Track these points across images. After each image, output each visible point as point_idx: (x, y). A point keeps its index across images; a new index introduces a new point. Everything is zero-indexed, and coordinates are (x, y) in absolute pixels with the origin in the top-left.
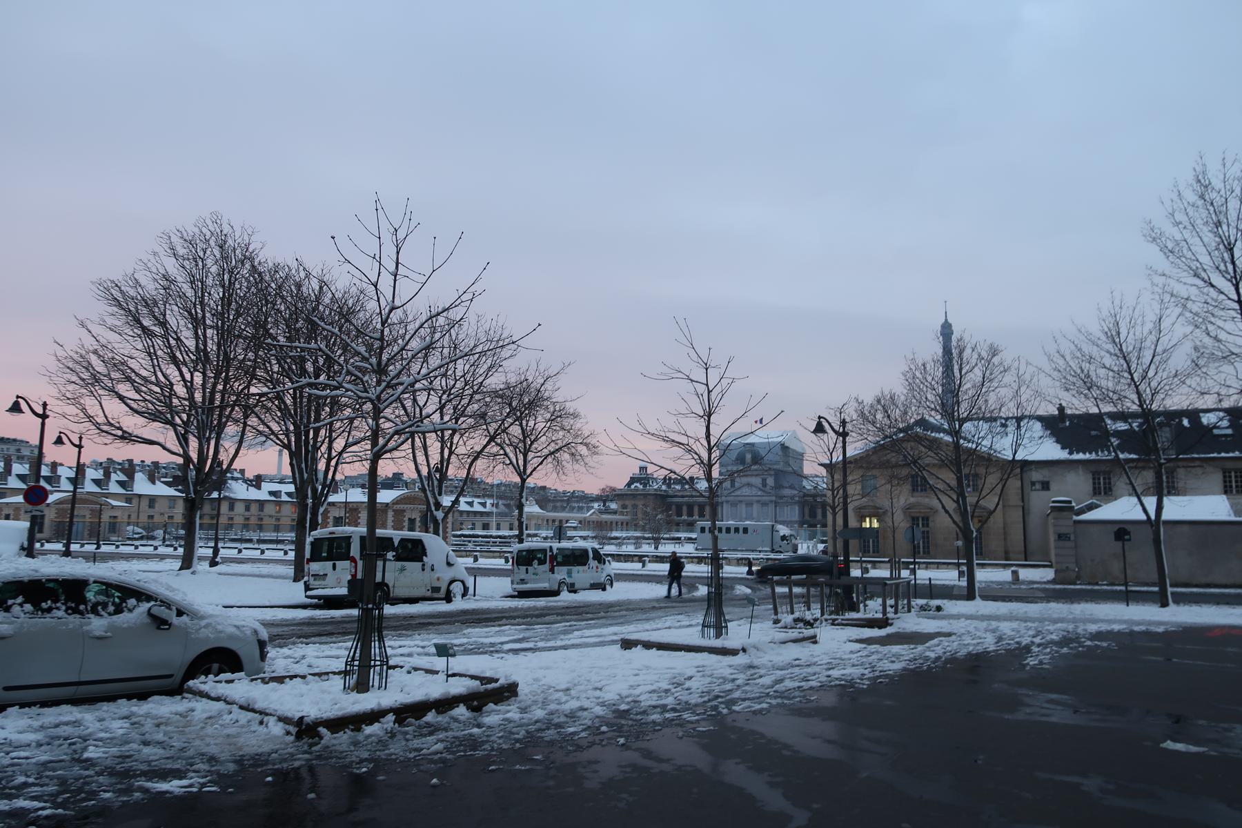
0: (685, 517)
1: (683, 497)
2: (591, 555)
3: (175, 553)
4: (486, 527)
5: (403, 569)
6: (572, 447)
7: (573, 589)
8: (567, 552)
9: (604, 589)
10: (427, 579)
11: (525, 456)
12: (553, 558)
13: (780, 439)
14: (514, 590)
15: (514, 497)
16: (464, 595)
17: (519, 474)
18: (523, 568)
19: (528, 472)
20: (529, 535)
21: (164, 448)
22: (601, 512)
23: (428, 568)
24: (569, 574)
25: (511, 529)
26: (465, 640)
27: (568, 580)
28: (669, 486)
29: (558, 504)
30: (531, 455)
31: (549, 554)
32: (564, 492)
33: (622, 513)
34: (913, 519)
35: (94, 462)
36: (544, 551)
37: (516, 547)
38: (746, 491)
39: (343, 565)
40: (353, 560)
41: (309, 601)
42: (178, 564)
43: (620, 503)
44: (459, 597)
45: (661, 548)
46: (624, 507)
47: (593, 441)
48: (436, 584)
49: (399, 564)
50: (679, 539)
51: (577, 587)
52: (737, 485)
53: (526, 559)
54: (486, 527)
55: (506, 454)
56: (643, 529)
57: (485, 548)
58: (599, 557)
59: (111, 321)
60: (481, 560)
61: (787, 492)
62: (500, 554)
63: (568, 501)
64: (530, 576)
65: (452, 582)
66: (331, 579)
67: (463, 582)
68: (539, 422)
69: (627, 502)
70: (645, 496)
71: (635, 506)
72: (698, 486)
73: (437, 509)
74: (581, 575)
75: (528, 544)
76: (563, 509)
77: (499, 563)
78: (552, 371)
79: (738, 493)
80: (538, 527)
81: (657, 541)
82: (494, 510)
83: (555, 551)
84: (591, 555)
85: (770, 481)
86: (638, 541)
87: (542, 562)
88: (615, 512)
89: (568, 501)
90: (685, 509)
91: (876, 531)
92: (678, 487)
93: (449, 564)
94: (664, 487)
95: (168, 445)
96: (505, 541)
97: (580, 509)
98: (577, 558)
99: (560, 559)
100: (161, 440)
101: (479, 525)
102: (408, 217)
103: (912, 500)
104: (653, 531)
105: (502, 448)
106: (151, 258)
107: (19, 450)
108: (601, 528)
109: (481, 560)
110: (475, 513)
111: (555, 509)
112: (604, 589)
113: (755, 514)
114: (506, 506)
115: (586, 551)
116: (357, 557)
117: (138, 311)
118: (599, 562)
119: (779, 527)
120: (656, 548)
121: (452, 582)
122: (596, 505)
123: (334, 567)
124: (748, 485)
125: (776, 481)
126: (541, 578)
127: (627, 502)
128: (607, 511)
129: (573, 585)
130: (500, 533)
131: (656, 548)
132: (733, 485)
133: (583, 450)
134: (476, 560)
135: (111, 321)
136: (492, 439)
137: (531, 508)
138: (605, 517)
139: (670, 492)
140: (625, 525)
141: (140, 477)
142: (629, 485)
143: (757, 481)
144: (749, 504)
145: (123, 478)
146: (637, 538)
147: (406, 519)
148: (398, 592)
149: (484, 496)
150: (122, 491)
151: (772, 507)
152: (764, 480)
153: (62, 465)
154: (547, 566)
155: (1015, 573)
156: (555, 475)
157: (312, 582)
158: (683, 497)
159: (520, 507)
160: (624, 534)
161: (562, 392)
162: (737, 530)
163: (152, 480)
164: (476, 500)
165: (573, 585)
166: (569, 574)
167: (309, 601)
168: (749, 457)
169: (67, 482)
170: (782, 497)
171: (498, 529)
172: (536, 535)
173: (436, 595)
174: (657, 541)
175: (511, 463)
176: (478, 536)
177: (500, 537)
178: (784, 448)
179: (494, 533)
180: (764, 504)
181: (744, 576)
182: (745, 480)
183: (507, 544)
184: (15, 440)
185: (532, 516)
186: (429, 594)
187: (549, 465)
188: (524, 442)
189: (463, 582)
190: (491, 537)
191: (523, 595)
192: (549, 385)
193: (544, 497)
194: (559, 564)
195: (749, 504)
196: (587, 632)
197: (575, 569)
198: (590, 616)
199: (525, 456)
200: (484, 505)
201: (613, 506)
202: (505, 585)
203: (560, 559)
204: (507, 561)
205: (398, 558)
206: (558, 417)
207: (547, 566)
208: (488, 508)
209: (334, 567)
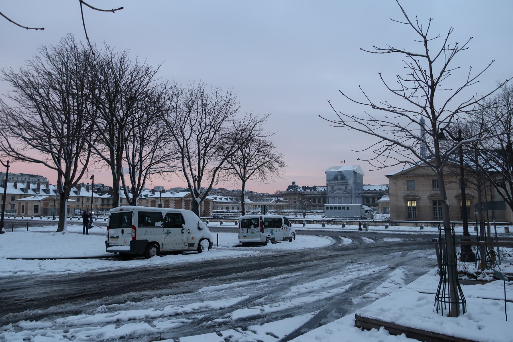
0: (317, 203)
1: (311, 195)
2: (283, 221)
3: (79, 221)
4: (227, 208)
5: (168, 233)
6: (270, 162)
7: (274, 241)
8: (269, 220)
9: (291, 241)
10: (185, 238)
11: (245, 169)
12: (263, 223)
13: (355, 169)
14: (240, 242)
15: (241, 195)
16: (210, 247)
17: (242, 179)
18: (245, 230)
19: (247, 176)
20: (246, 212)
21: (46, 165)
22: (276, 202)
23: (185, 232)
24: (272, 232)
25: (238, 209)
26: (196, 305)
27: (271, 236)
28: (305, 190)
29: (258, 199)
30: (247, 168)
31: (260, 221)
32: (260, 194)
33: (285, 202)
34: (434, 201)
36: (257, 220)
37: (241, 217)
38: (338, 192)
39: (128, 231)
40: (134, 228)
41: (110, 254)
42: (56, 228)
43: (284, 197)
44: (206, 249)
45: (306, 217)
46: (286, 199)
47: (281, 160)
48: (191, 242)
49: (166, 229)
50: (313, 212)
51: (276, 239)
52: (335, 189)
53: (247, 224)
54: (227, 208)
55: (234, 168)
56: (299, 209)
57: (226, 218)
58: (288, 223)
59: (13, 95)
60: (224, 223)
62: (233, 220)
63: (262, 197)
64: (249, 234)
65: (201, 240)
66: (120, 240)
67: (208, 240)
68: (251, 150)
69: (287, 197)
70: (295, 194)
71: (290, 199)
72: (317, 190)
73: (197, 197)
74: (278, 233)
75: (247, 216)
76: (260, 200)
77: (232, 225)
78: (259, 119)
79: (335, 193)
80: (250, 208)
81: (304, 214)
82: (231, 201)
83: (263, 220)
84: (283, 221)
86: (295, 214)
87: (256, 226)
88: (282, 202)
89: (262, 197)
90: (317, 200)
91: (414, 208)
92: (309, 191)
93: (199, 229)
94: (303, 191)
95: (48, 163)
96: (235, 214)
97: (267, 200)
98: (276, 223)
99: (266, 224)
100: (44, 161)
101: (225, 207)
103: (433, 192)
104: (302, 209)
105: (232, 165)
106: (35, 59)
107: (39, 180)
108: (279, 208)
109: (224, 223)
110: (223, 203)
111: (256, 200)
112: (291, 241)
113: (343, 201)
114: (236, 199)
115: (281, 219)
116: (136, 225)
117: (28, 88)
118: (288, 225)
119: (364, 206)
120: (304, 217)
121: (201, 240)
122: (274, 199)
123: (123, 233)
124: (340, 189)
126: (256, 235)
127: (287, 197)
128: (279, 201)
129: (274, 239)
130: (233, 211)
131: (304, 217)
132: (333, 189)
133: (276, 165)
134: (222, 223)
135: (13, 95)
136: (226, 158)
137: (247, 200)
138: (278, 203)
139: (306, 193)
140: (288, 207)
141: (82, 189)
142: (288, 190)
144: (340, 197)
145: (76, 189)
146: (295, 212)
148: (166, 247)
149: (226, 196)
150: (75, 195)
153: (51, 184)
154: (259, 228)
155: (507, 229)
156: (260, 179)
157: (111, 242)
158: (311, 195)
159: (243, 200)
160: (291, 211)
161: (264, 132)
162: (344, 208)
163: (88, 190)
164: (223, 197)
165: (274, 239)
166: (272, 232)
167: (110, 254)
168: (339, 177)
169: (53, 192)
171: (233, 209)
172: (249, 212)
173: (191, 248)
174: (304, 214)
175: (237, 172)
176: (224, 212)
177: (233, 212)
178: (355, 173)
179: (231, 211)
181: (357, 231)
182: (338, 187)
183: (237, 216)
184: (37, 176)
185: (247, 204)
186: (187, 248)
187: (257, 173)
188: (244, 161)
189: (208, 240)
190: (229, 212)
191: (246, 245)
192: (257, 128)
193: (252, 195)
194: (266, 227)
195: (340, 197)
196: (303, 287)
197: (275, 229)
198: (294, 266)
199: (245, 169)
200: (226, 199)
201: (281, 199)
202: (234, 238)
203: (266, 224)
204: (236, 224)
205: (165, 226)
206: (262, 146)
207: (259, 228)
208: (229, 200)
209: (123, 233)
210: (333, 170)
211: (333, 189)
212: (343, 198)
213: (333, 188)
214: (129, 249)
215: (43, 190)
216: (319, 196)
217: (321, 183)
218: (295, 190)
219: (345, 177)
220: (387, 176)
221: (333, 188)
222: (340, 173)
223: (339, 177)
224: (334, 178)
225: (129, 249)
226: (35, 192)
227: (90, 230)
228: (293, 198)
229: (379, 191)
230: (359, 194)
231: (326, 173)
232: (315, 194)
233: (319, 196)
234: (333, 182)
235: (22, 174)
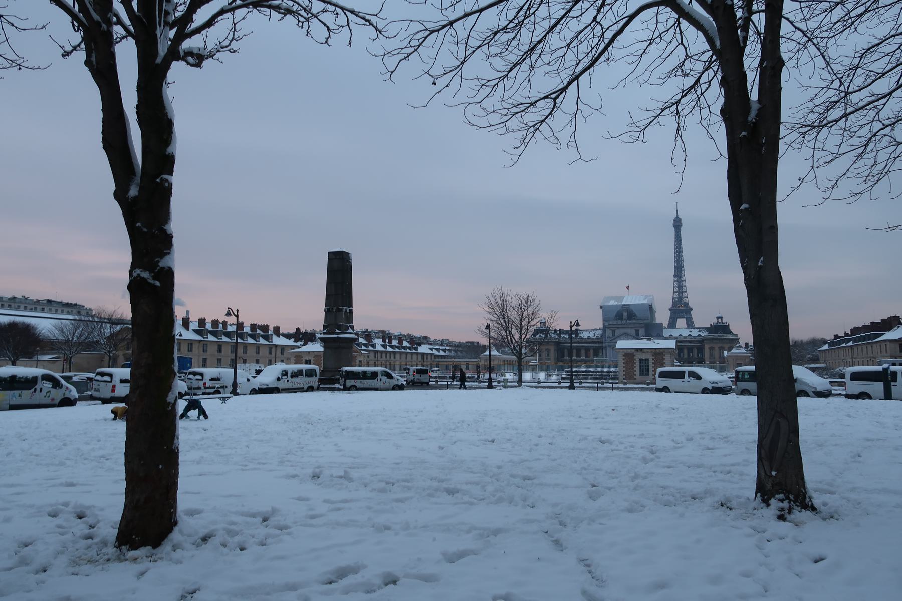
0: (583, 357)
82: (382, 349)
90: (583, 352)
132: (614, 334)
168: (625, 314)
182: (622, 331)
184: (76, 304)
210: (612, 303)
211: (614, 334)
213: (613, 332)
215: (194, 330)
216: (586, 345)
217: (592, 324)
218: (546, 335)
221: (613, 332)
222: (626, 307)
223: (625, 314)
224: (616, 316)
226: (202, 335)
228: (716, 346)
229: (689, 338)
231: (601, 307)
232: (579, 343)
233: (586, 345)
235: (48, 301)
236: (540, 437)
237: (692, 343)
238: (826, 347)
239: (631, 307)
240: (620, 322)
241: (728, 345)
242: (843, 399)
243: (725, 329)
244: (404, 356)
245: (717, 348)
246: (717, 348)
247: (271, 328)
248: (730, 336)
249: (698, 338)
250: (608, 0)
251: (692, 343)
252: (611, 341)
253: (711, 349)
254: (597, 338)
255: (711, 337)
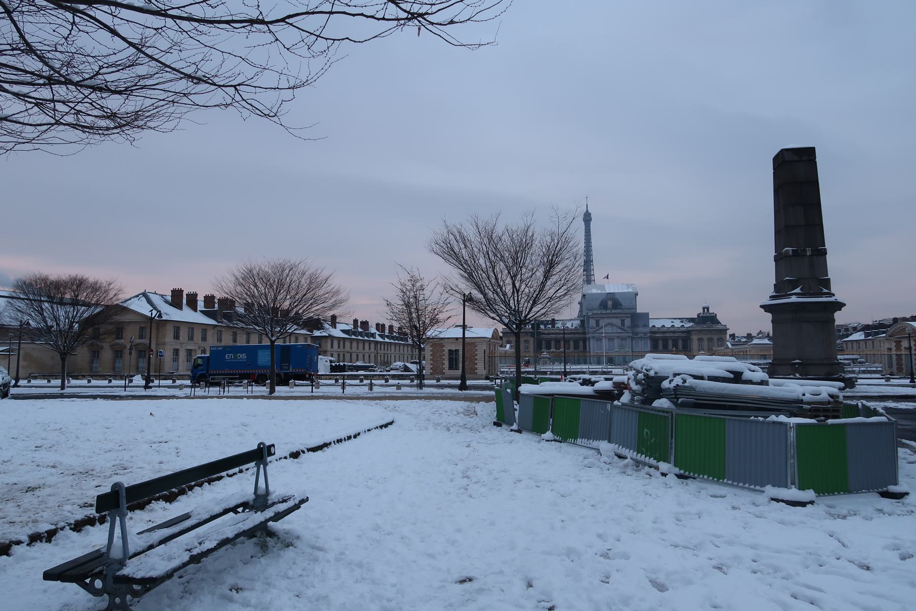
35: (497, 266)
38: (609, 329)
61: (641, 329)
85: (628, 322)
90: (553, 343)
102: (329, 64)
125: (632, 322)
143: (618, 322)
147: (446, 351)
151: (629, 341)
152: (623, 322)
168: (610, 303)
170: (636, 334)
180: (623, 339)
182: (607, 321)
212: (616, 341)
214: (899, 449)
215: (201, 311)
219: (621, 305)
220: (761, 306)
222: (611, 296)
223: (610, 303)
224: (601, 305)
225: (899, 449)
227: (151, 384)
228: (705, 337)
230: (645, 334)
234: (599, 312)
236: (161, 463)
237: (677, 335)
238: (858, 336)
239: (617, 296)
240: (604, 312)
241: (718, 336)
242: (378, 431)
243: (713, 319)
244: (397, 348)
245: (705, 340)
246: (705, 340)
247: (729, 333)
248: (719, 327)
249: (682, 329)
250: (466, 1)
251: (677, 335)
252: (594, 332)
253: (700, 340)
254: (576, 328)
255: (698, 328)
